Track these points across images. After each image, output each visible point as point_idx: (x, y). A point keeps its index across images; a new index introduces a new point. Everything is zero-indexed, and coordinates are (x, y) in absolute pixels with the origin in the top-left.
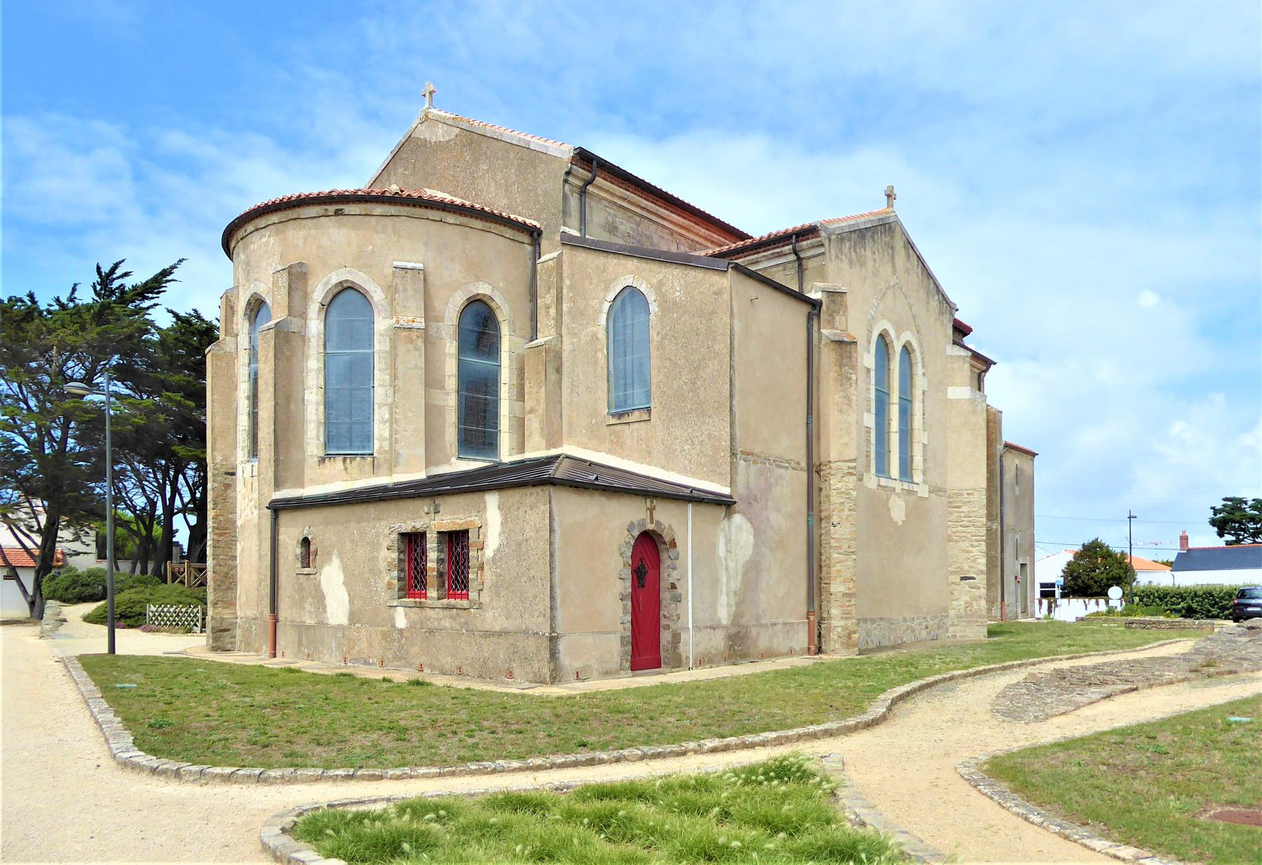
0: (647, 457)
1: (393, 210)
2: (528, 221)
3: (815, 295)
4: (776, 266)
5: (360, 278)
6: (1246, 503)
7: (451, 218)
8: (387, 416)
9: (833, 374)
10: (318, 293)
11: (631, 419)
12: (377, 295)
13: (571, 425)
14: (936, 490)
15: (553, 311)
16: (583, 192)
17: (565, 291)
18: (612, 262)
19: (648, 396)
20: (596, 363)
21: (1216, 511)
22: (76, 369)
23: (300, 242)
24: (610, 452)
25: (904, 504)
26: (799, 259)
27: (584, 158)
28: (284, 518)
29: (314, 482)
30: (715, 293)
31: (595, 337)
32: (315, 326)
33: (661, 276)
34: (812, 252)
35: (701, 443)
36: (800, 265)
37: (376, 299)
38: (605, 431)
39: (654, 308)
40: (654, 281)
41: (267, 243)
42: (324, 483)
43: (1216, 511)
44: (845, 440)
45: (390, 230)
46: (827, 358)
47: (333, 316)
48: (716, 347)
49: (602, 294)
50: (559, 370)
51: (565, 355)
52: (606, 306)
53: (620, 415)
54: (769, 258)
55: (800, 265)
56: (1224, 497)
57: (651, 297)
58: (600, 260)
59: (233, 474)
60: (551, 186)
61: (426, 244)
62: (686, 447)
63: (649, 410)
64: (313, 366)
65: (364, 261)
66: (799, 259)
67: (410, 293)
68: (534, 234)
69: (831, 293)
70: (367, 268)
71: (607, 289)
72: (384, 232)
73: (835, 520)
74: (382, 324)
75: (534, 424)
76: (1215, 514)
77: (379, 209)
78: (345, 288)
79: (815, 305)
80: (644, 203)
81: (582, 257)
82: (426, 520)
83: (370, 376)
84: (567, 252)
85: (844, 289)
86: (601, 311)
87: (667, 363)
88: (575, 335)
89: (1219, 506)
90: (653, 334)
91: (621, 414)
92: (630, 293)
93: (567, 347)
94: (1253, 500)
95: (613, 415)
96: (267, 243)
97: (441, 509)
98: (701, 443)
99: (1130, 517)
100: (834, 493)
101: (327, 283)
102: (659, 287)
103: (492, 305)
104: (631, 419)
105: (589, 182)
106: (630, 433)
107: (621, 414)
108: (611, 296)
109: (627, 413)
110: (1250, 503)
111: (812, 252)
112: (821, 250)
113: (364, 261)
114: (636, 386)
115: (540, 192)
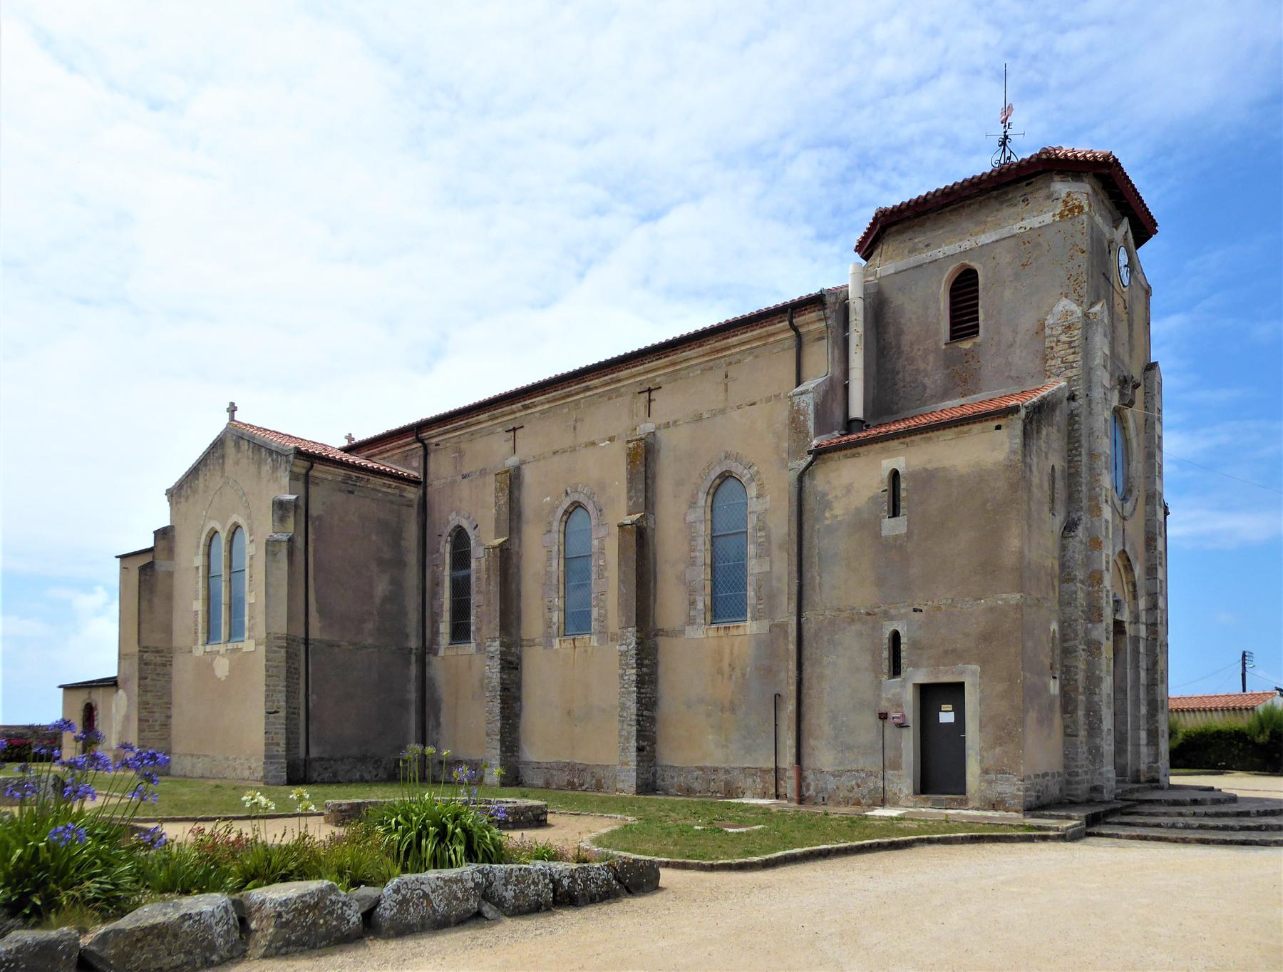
25: (228, 662)
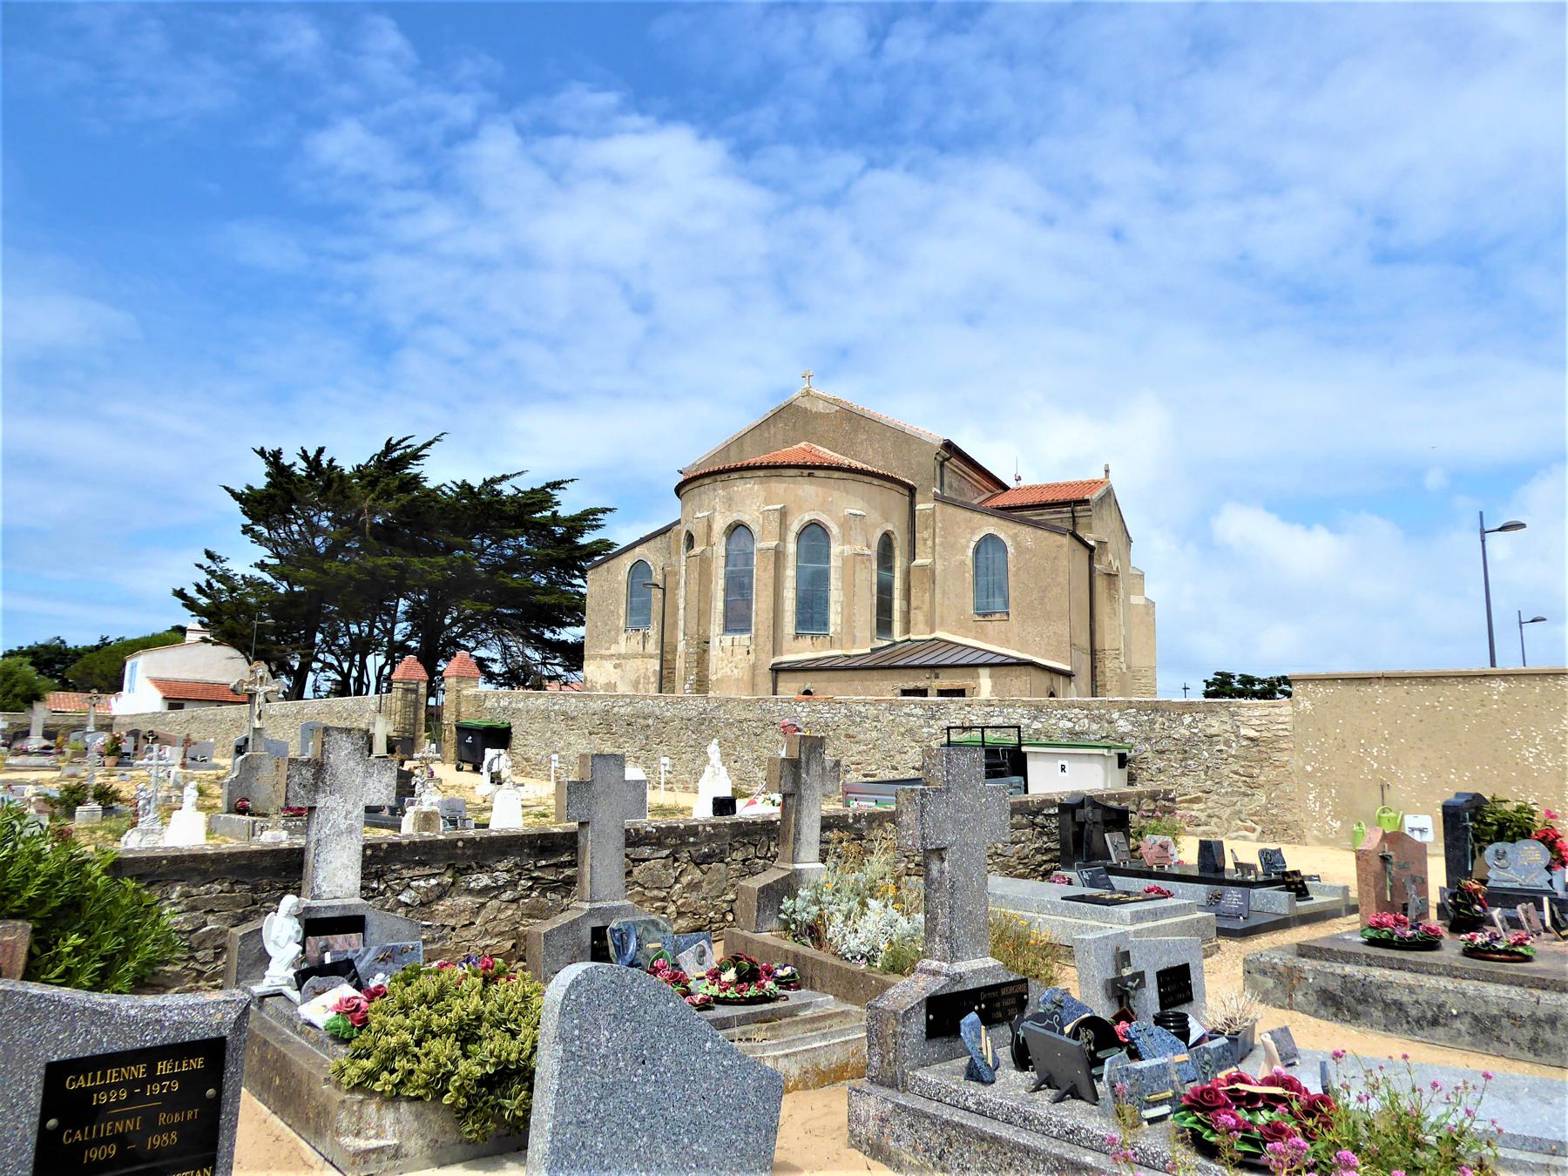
0: (1006, 642)
1: (845, 475)
2: (906, 480)
3: (1092, 543)
4: (1061, 517)
5: (824, 518)
6: (1233, 677)
7: (876, 482)
8: (839, 610)
9: (1105, 595)
10: (795, 526)
11: (993, 618)
12: (834, 530)
13: (942, 618)
14: (1129, 668)
15: (930, 543)
16: (942, 465)
17: (937, 530)
18: (977, 517)
19: (1007, 604)
20: (964, 580)
21: (1208, 684)
22: (330, 514)
23: (782, 492)
24: (976, 638)
26: (1074, 517)
27: (949, 446)
28: (782, 676)
29: (790, 652)
30: (1057, 546)
31: (963, 563)
32: (791, 547)
33: (1016, 531)
34: (1082, 514)
35: (1049, 637)
36: (1074, 521)
37: (834, 532)
38: (971, 623)
39: (1011, 550)
40: (1011, 534)
41: (752, 489)
42: (798, 653)
43: (1208, 684)
44: (1113, 636)
45: (842, 488)
46: (1100, 584)
47: (801, 542)
48: (1059, 579)
49: (969, 536)
50: (934, 583)
51: (937, 572)
52: (972, 545)
53: (985, 615)
54: (1051, 513)
55: (1074, 521)
56: (211, 549)
57: (1009, 543)
58: (968, 514)
59: (708, 643)
60: (930, 464)
61: (862, 499)
62: (1037, 639)
63: (1008, 614)
64: (790, 573)
65: (825, 507)
66: (1074, 517)
67: (858, 530)
68: (912, 490)
69: (1099, 542)
70: (828, 511)
71: (973, 533)
72: (839, 489)
73: (1108, 687)
74: (835, 549)
75: (918, 617)
76: (1207, 687)
77: (836, 474)
78: (814, 524)
79: (1091, 549)
80: (966, 469)
81: (951, 510)
82: (928, 682)
83: (827, 579)
84: (938, 505)
85: (1106, 540)
86: (968, 547)
87: (1021, 586)
88: (945, 560)
89: (1210, 680)
90: (1010, 566)
91: (985, 613)
92: (990, 539)
93: (939, 568)
94: (1217, 674)
95: (979, 614)
96: (752, 489)
97: (940, 676)
98: (1049, 637)
99: (1185, 689)
100: (1107, 670)
101: (802, 520)
102: (1014, 537)
103: (893, 537)
104: (993, 618)
105: (948, 459)
106: (993, 627)
107: (985, 613)
108: (977, 538)
109: (991, 614)
110: (1237, 678)
111: (1082, 514)
112: (1089, 513)
113: (825, 507)
114: (997, 595)
115: (913, 461)
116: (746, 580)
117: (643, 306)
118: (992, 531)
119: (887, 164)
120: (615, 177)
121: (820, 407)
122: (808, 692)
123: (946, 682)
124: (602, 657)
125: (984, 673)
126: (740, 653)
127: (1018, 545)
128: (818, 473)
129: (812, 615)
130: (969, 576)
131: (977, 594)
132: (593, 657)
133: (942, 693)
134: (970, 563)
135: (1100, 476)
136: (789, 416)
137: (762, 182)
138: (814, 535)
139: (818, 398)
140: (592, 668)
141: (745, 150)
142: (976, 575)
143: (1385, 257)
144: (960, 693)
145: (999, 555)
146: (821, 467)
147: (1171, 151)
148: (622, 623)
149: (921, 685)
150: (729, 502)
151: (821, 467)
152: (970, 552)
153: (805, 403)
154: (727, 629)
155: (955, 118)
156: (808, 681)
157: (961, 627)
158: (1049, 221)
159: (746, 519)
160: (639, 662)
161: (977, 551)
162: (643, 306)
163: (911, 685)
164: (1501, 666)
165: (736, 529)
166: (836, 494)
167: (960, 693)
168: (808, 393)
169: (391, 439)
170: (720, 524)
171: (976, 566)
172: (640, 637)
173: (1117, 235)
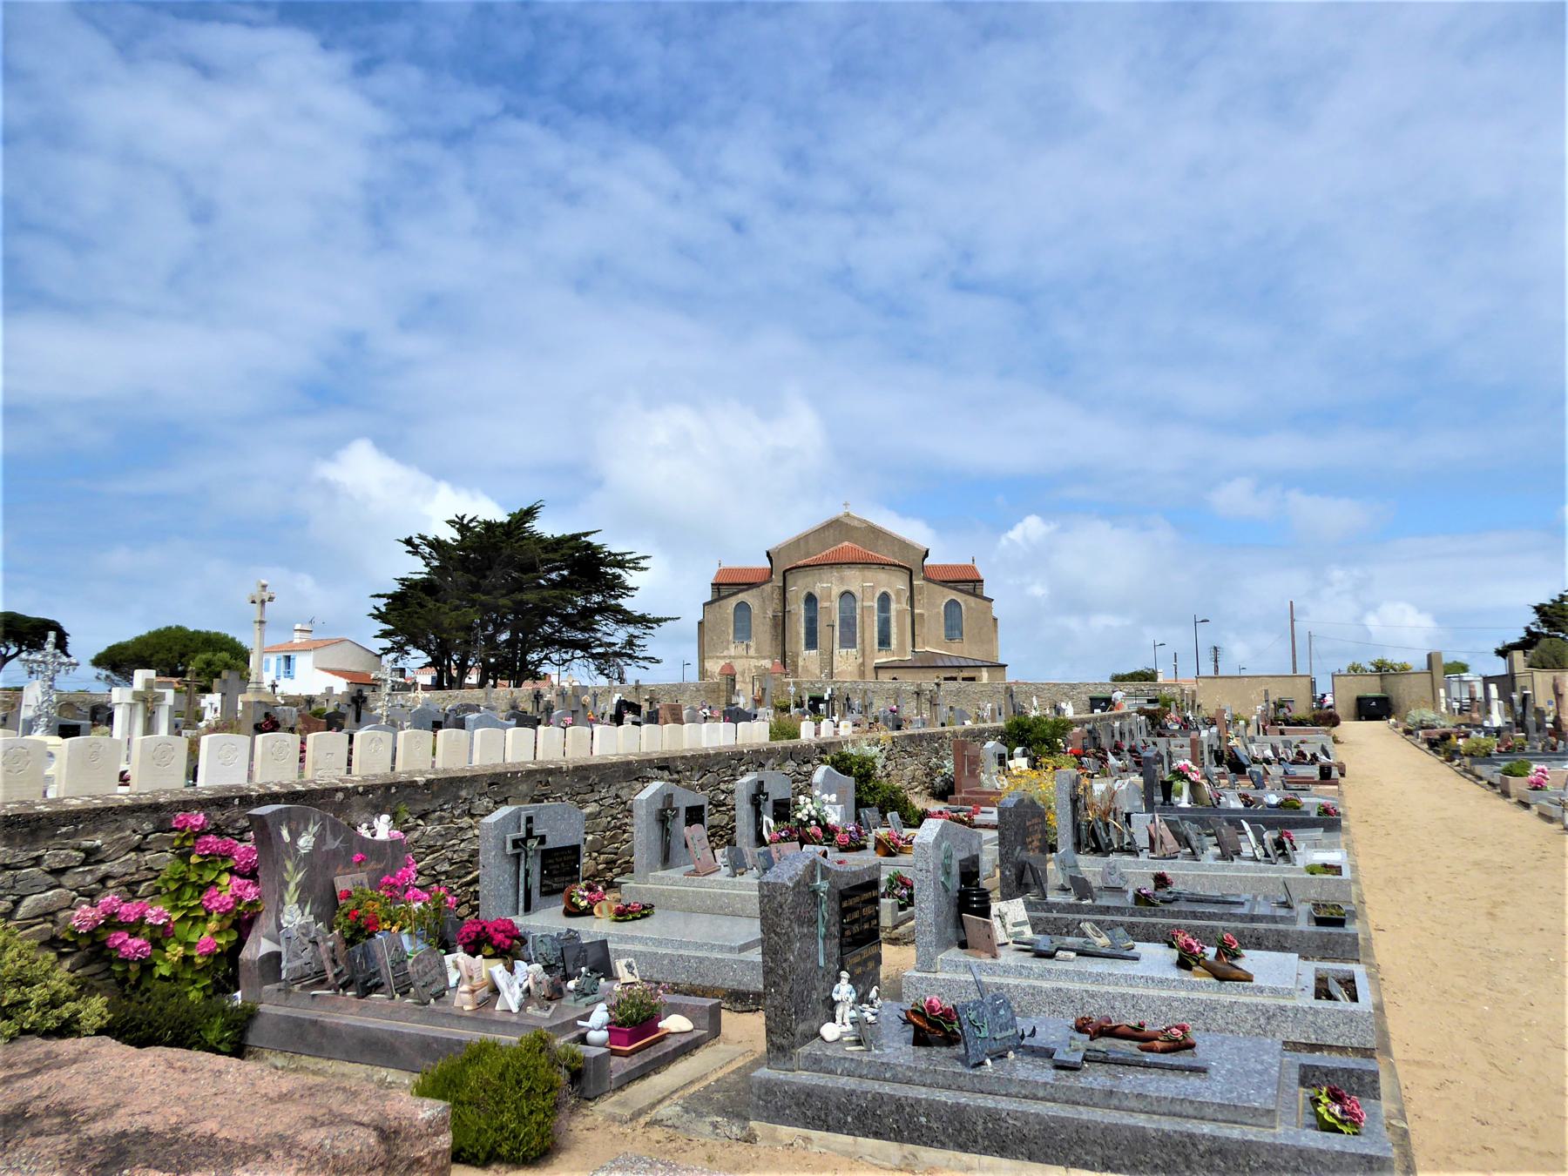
5: (889, 591)
12: (893, 597)
28: (880, 671)
31: (939, 613)
57: (962, 604)
70: (890, 587)
91: (951, 638)
92: (953, 603)
102: (965, 601)
107: (951, 638)
116: (851, 621)
117: (203, 214)
118: (954, 597)
119: (519, 114)
120: (205, 70)
121: (856, 523)
122: (895, 679)
123: (966, 674)
124: (718, 657)
125: (984, 669)
126: (852, 659)
127: (966, 605)
128: (887, 567)
129: (884, 641)
130: (942, 620)
131: (946, 630)
132: (710, 658)
133: (964, 679)
134: (942, 613)
135: (970, 563)
136: (838, 527)
137: (379, 102)
138: (885, 599)
139: (854, 518)
140: (711, 664)
141: (365, 68)
142: (946, 619)
143: (962, 286)
144: (973, 679)
145: (957, 610)
146: (888, 565)
147: (797, 160)
148: (731, 637)
149: (954, 675)
150: (842, 580)
151: (888, 565)
152: (943, 608)
153: (846, 520)
154: (841, 646)
155: (602, 81)
156: (895, 673)
157: (938, 646)
158: (676, 198)
159: (852, 589)
160: (744, 660)
161: (946, 606)
162: (203, 214)
163: (948, 675)
164: (1220, 674)
165: (846, 595)
166: (893, 578)
167: (973, 679)
168: (848, 515)
169: (529, 513)
170: (836, 590)
171: (945, 615)
172: (744, 646)
173: (738, 226)
